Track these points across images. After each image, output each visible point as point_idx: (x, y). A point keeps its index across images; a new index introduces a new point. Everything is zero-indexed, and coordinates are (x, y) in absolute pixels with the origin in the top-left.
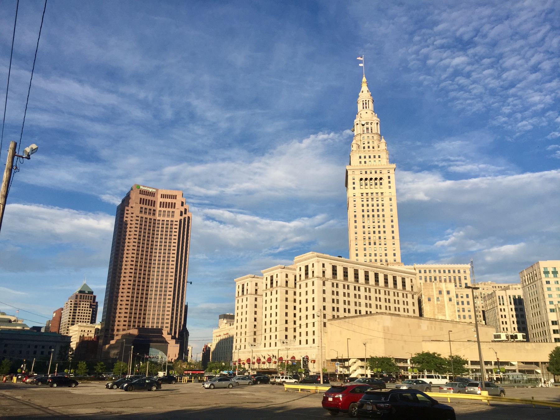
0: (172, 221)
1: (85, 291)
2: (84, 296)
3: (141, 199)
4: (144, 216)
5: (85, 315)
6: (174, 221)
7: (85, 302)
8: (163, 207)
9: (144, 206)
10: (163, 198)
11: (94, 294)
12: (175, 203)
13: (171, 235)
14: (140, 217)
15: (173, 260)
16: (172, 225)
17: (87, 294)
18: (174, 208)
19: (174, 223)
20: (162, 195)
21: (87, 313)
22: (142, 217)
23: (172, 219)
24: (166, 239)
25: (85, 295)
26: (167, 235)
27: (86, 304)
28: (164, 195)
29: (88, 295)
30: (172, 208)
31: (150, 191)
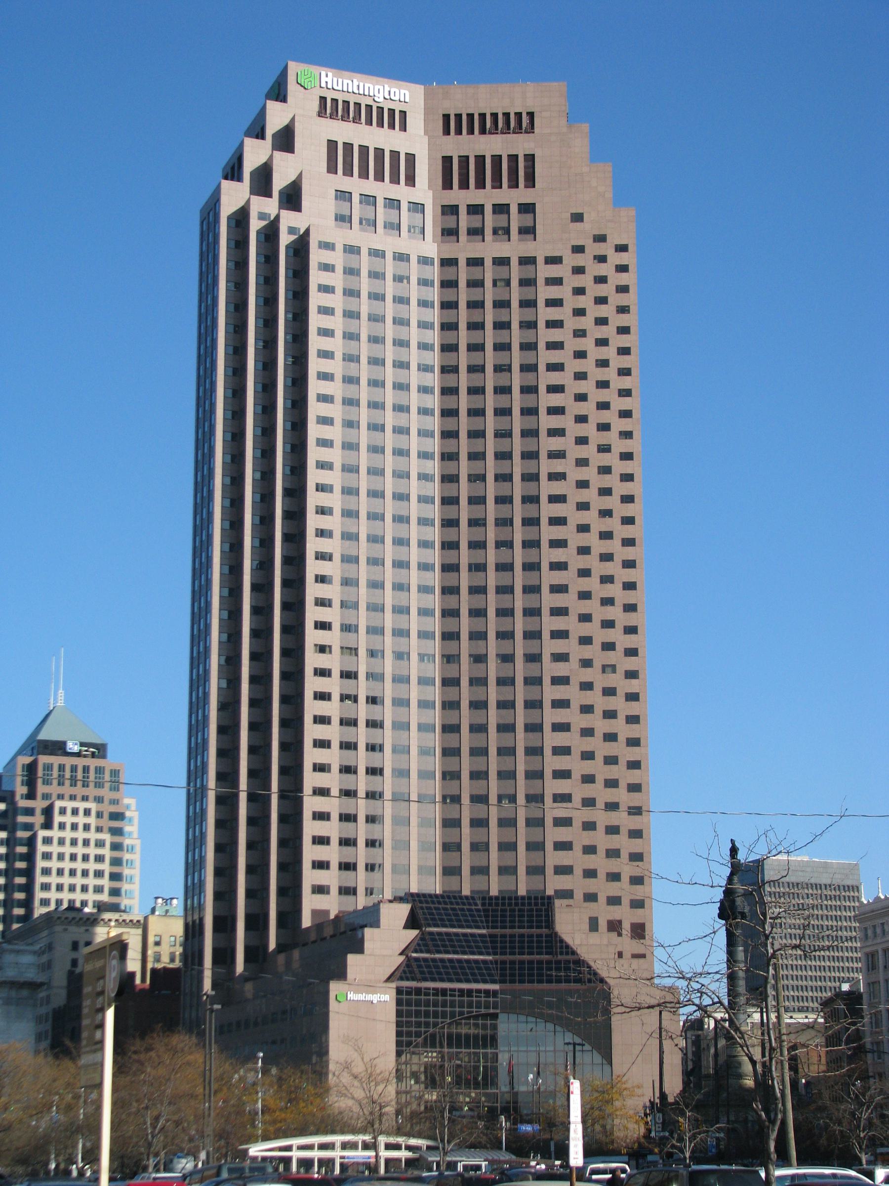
0: (527, 261)
1: (64, 743)
2: (62, 768)
3: (332, 145)
4: (366, 240)
5: (80, 850)
6: (540, 261)
7: (73, 798)
8: (464, 184)
9: (356, 185)
10: (459, 132)
11: (111, 761)
12: (530, 159)
13: (530, 455)
14: (339, 248)
15: (555, 484)
16: (527, 282)
17: (78, 755)
18: (531, 181)
19: (544, 271)
20: (446, 117)
21: (86, 843)
22: (352, 250)
23: (528, 248)
24: (478, 590)
25: (68, 761)
26: (498, 478)
27: (75, 812)
28: (459, 117)
29: (80, 762)
30: (514, 184)
31: (127, 829)
